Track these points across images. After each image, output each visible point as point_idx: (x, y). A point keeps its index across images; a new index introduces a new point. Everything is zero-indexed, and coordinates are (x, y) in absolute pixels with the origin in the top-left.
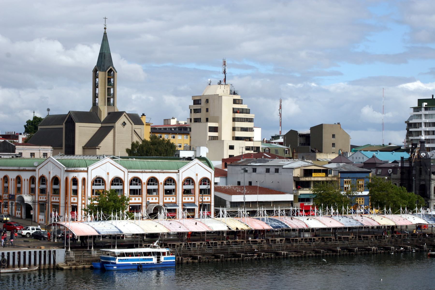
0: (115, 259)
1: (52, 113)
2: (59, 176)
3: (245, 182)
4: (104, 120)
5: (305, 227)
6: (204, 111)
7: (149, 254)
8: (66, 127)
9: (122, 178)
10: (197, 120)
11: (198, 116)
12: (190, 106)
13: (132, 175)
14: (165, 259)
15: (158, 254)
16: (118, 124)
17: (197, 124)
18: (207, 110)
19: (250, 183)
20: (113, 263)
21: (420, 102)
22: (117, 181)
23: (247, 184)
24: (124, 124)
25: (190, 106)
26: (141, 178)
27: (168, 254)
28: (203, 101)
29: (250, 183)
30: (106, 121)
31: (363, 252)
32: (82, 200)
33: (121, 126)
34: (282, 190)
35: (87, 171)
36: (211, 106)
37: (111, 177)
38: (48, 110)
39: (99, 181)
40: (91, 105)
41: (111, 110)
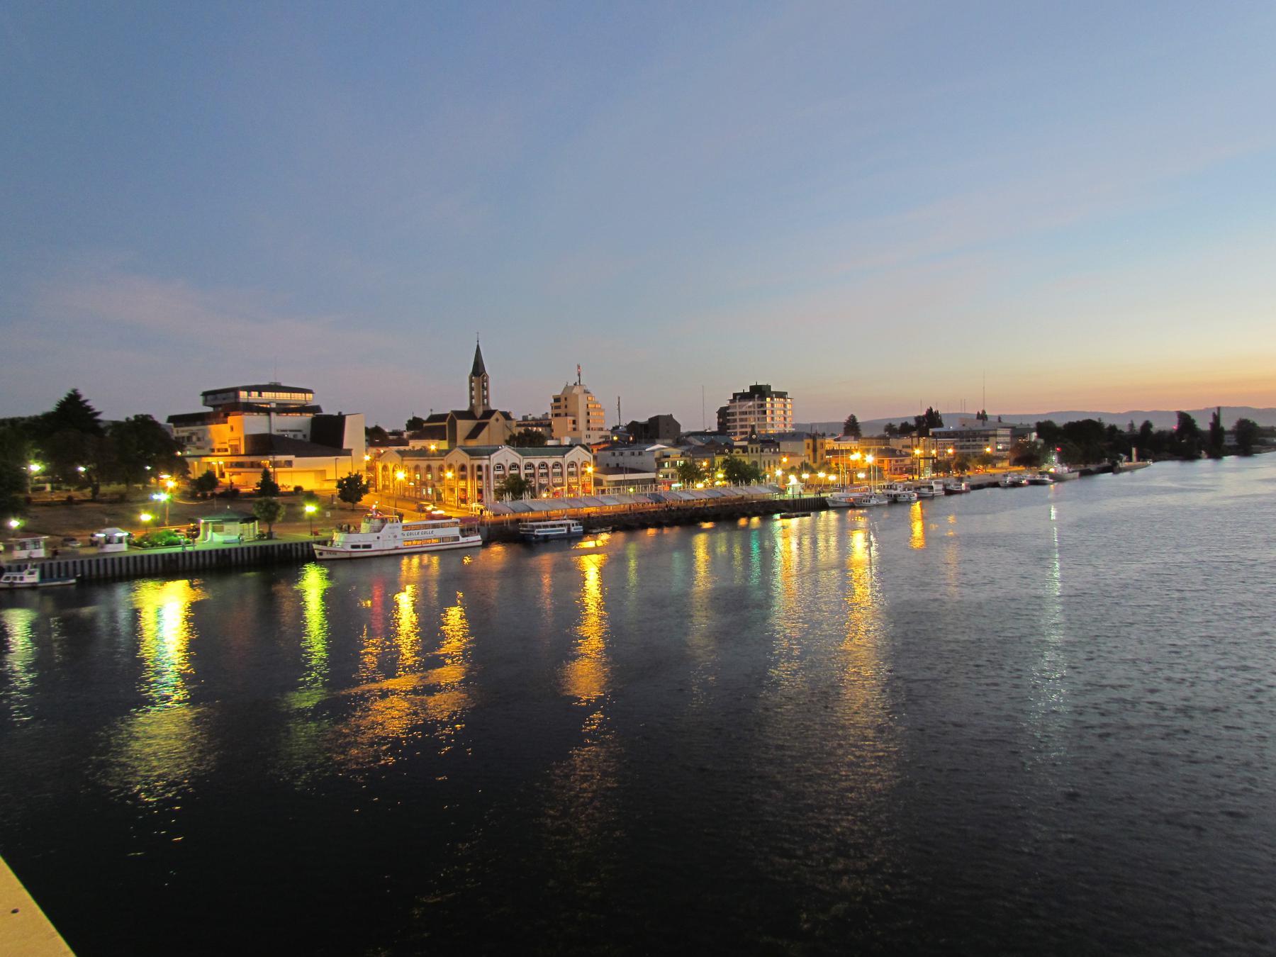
0: (533, 531)
1: (434, 413)
2: (465, 463)
3: (613, 464)
4: (472, 419)
5: (651, 506)
6: (563, 407)
7: (561, 525)
8: (449, 425)
9: (518, 463)
10: (557, 415)
11: (558, 411)
12: (551, 404)
13: (526, 461)
14: (575, 529)
15: (569, 525)
16: (492, 420)
17: (229, 429)
18: (566, 407)
19: (618, 465)
20: (532, 535)
21: (735, 395)
22: (514, 466)
23: (615, 466)
24: (497, 420)
25: (551, 404)
26: (547, 462)
27: (577, 525)
28: (563, 400)
29: (618, 465)
30: (482, 418)
31: (374, 617)
32: (486, 483)
33: (495, 422)
34: (646, 470)
35: (489, 459)
36: (569, 403)
37: (510, 463)
38: (431, 410)
39: (500, 467)
40: (469, 405)
41: (486, 409)
